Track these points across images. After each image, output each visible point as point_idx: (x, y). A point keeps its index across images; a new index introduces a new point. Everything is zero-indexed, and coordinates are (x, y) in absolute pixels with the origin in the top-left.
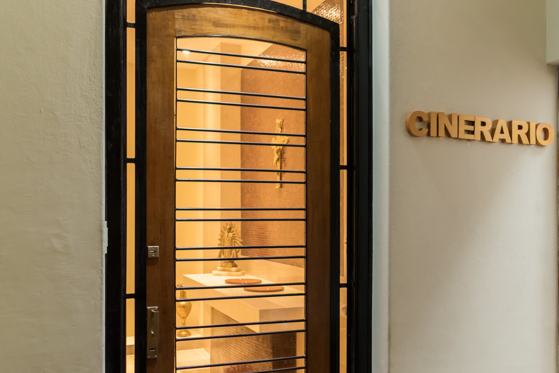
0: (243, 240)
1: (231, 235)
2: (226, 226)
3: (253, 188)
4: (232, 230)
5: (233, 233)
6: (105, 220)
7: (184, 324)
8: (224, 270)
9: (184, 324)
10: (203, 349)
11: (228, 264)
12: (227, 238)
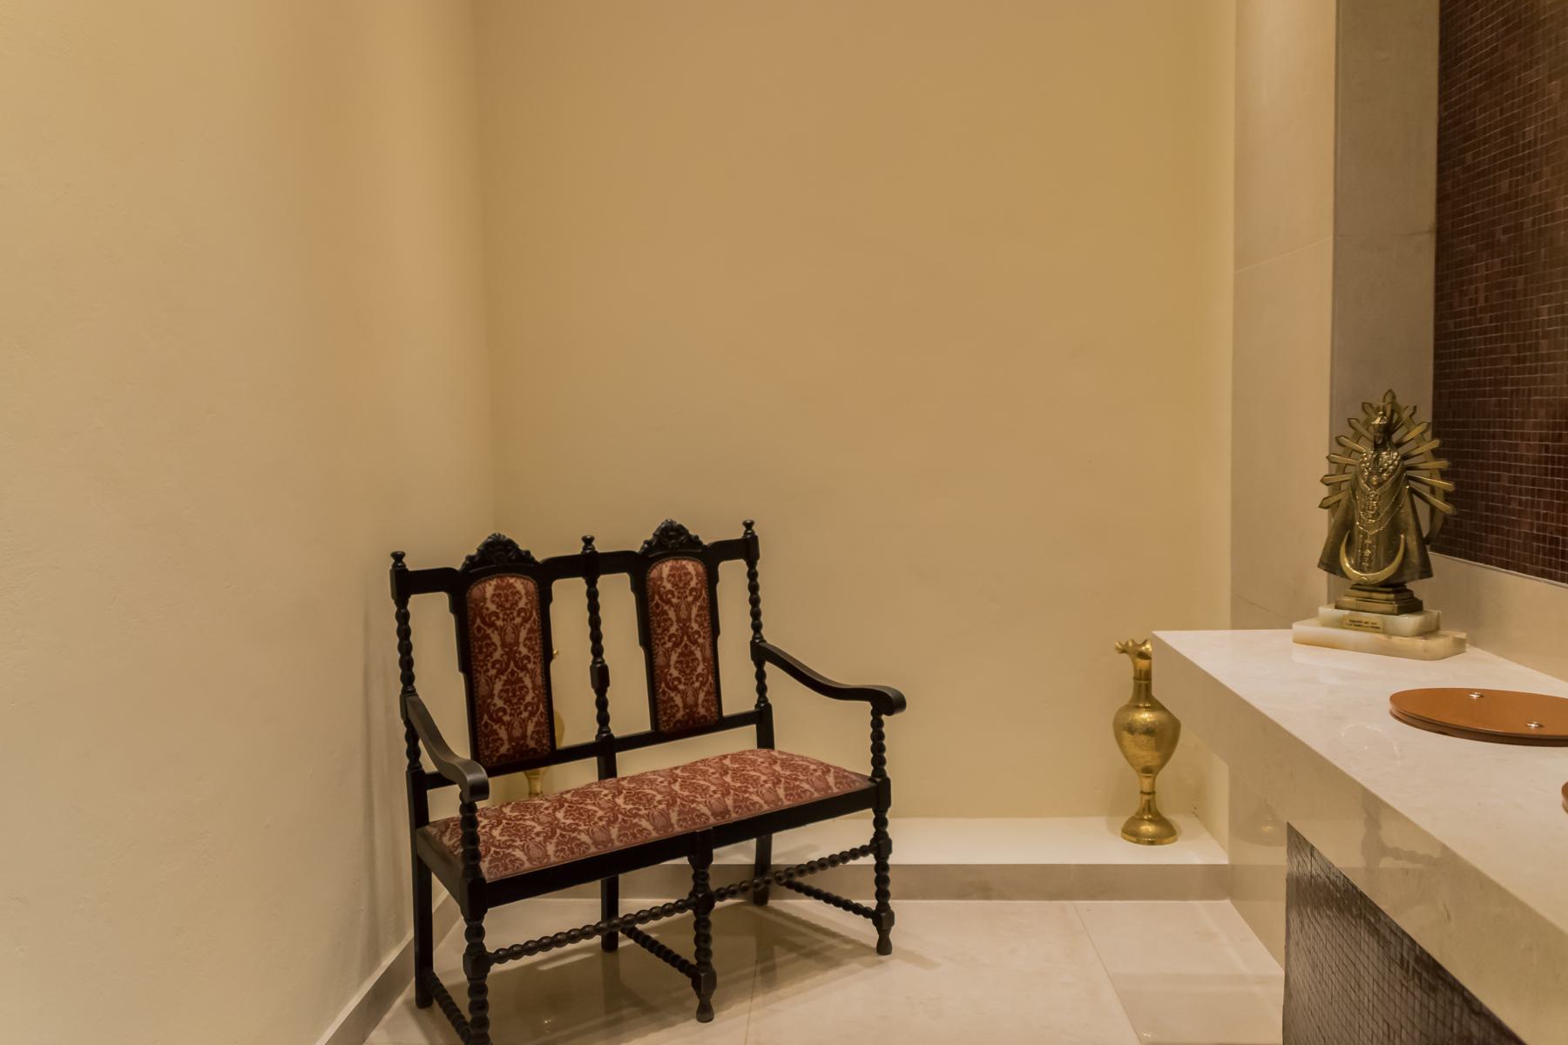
0: (1456, 484)
1: (1389, 458)
2: (1362, 417)
3: (1528, 221)
4: (1395, 437)
5: (1403, 450)
6: (1290, 628)
7: (1149, 794)
8: (1357, 625)
9: (1149, 794)
10: (1227, 902)
11: (1375, 595)
12: (1371, 474)
